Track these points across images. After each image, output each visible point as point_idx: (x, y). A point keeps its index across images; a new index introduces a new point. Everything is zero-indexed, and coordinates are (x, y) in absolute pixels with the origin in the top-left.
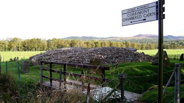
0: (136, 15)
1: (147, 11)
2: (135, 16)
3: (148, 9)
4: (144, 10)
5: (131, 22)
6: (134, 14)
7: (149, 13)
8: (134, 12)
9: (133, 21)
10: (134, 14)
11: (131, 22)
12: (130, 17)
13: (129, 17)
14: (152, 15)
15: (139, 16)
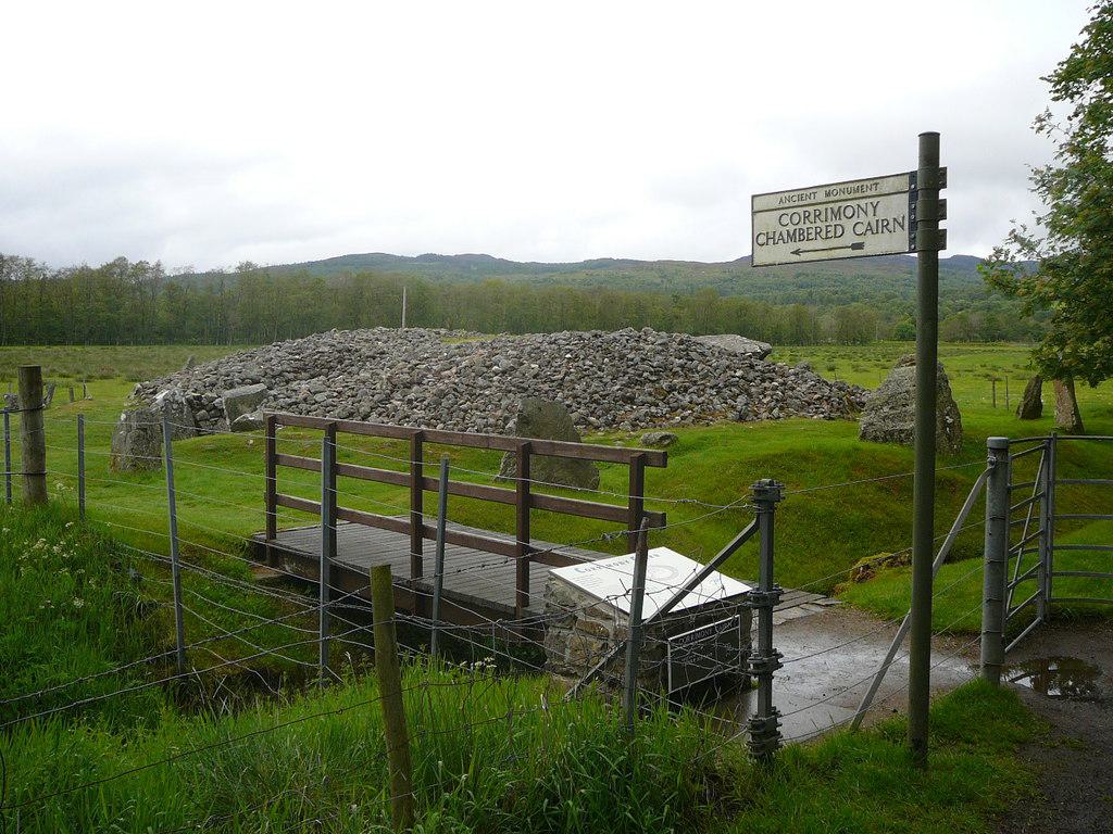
0: (819, 224)
1: (870, 209)
2: (813, 226)
3: (875, 200)
4: (854, 203)
5: (797, 252)
6: (812, 218)
7: (881, 215)
8: (811, 209)
9: (803, 245)
10: (812, 218)
11: (797, 252)
12: (791, 228)
13: (784, 230)
14: (891, 227)
15: (831, 229)
